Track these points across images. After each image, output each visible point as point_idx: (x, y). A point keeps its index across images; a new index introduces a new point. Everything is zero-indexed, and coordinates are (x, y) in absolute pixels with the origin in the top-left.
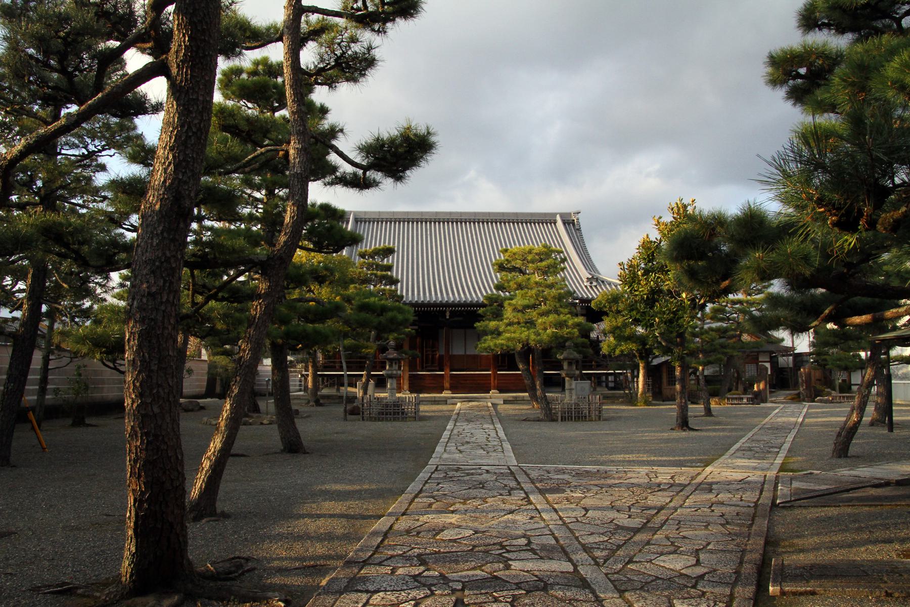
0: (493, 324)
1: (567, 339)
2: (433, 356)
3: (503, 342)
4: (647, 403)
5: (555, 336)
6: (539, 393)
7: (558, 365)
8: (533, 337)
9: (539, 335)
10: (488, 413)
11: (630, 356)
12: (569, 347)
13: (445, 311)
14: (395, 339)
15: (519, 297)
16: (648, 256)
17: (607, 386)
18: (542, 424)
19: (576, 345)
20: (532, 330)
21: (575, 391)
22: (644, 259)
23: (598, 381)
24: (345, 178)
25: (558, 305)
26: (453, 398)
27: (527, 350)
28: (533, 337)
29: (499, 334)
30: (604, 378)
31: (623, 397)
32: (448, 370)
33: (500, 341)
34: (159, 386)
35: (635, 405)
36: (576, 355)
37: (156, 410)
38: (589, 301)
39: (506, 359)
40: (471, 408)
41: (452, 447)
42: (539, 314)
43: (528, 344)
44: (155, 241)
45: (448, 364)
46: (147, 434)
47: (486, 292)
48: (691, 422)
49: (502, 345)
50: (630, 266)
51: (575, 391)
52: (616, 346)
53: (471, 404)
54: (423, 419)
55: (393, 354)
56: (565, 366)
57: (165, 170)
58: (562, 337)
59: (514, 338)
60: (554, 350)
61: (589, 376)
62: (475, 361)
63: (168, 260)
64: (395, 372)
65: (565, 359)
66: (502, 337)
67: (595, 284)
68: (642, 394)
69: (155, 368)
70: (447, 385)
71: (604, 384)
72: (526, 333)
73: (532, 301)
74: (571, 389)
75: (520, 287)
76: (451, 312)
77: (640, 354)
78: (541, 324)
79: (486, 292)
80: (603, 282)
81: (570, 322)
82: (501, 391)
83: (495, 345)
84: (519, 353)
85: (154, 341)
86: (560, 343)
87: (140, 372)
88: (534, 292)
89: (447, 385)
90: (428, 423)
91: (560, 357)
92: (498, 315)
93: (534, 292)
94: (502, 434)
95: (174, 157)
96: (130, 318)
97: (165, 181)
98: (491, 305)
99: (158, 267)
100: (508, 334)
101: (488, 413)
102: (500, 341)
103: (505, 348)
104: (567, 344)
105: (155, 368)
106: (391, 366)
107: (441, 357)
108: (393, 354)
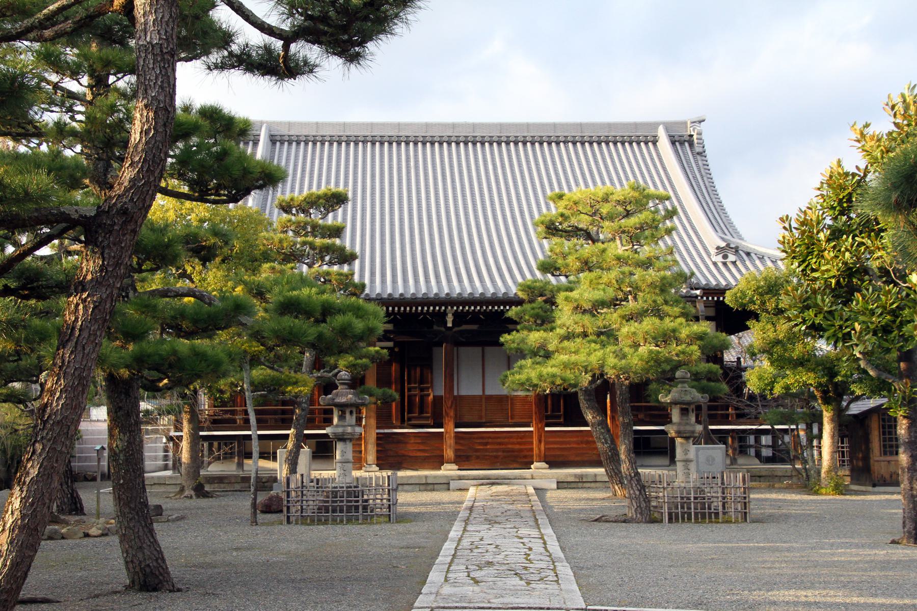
0: (535, 337)
1: (678, 366)
2: (423, 398)
3: (554, 370)
4: (840, 489)
5: (655, 360)
6: (625, 467)
7: (661, 415)
8: (612, 361)
9: (624, 356)
11: (805, 397)
12: (683, 381)
13: (445, 314)
16: (840, 202)
17: (758, 455)
20: (610, 348)
21: (696, 464)
22: (833, 208)
23: (740, 445)
25: (660, 300)
26: (460, 478)
27: (602, 387)
28: (612, 361)
29: (548, 356)
30: (752, 439)
31: (791, 477)
33: (549, 369)
35: (816, 493)
36: (695, 395)
38: (721, 292)
39: (561, 405)
40: (495, 497)
42: (623, 317)
43: (602, 375)
45: (452, 414)
49: (554, 376)
50: (803, 224)
51: (696, 464)
53: (496, 489)
54: (403, 518)
55: (344, 395)
56: (675, 415)
58: (668, 361)
59: (575, 364)
60: (653, 386)
61: (721, 437)
62: (500, 407)
64: (349, 430)
65: (674, 403)
66: (551, 362)
67: (732, 258)
68: (829, 471)
70: (449, 453)
71: (752, 451)
72: (599, 354)
73: (611, 293)
74: (687, 461)
76: (456, 314)
77: (825, 393)
80: (748, 254)
81: (684, 333)
82: (553, 464)
83: (540, 377)
84: (586, 391)
86: (667, 374)
91: (665, 398)
92: (544, 320)
93: (613, 275)
94: (554, 547)
100: (560, 356)
101: (527, 507)
102: (549, 369)
103: (558, 382)
104: (678, 374)
106: (342, 417)
108: (344, 395)
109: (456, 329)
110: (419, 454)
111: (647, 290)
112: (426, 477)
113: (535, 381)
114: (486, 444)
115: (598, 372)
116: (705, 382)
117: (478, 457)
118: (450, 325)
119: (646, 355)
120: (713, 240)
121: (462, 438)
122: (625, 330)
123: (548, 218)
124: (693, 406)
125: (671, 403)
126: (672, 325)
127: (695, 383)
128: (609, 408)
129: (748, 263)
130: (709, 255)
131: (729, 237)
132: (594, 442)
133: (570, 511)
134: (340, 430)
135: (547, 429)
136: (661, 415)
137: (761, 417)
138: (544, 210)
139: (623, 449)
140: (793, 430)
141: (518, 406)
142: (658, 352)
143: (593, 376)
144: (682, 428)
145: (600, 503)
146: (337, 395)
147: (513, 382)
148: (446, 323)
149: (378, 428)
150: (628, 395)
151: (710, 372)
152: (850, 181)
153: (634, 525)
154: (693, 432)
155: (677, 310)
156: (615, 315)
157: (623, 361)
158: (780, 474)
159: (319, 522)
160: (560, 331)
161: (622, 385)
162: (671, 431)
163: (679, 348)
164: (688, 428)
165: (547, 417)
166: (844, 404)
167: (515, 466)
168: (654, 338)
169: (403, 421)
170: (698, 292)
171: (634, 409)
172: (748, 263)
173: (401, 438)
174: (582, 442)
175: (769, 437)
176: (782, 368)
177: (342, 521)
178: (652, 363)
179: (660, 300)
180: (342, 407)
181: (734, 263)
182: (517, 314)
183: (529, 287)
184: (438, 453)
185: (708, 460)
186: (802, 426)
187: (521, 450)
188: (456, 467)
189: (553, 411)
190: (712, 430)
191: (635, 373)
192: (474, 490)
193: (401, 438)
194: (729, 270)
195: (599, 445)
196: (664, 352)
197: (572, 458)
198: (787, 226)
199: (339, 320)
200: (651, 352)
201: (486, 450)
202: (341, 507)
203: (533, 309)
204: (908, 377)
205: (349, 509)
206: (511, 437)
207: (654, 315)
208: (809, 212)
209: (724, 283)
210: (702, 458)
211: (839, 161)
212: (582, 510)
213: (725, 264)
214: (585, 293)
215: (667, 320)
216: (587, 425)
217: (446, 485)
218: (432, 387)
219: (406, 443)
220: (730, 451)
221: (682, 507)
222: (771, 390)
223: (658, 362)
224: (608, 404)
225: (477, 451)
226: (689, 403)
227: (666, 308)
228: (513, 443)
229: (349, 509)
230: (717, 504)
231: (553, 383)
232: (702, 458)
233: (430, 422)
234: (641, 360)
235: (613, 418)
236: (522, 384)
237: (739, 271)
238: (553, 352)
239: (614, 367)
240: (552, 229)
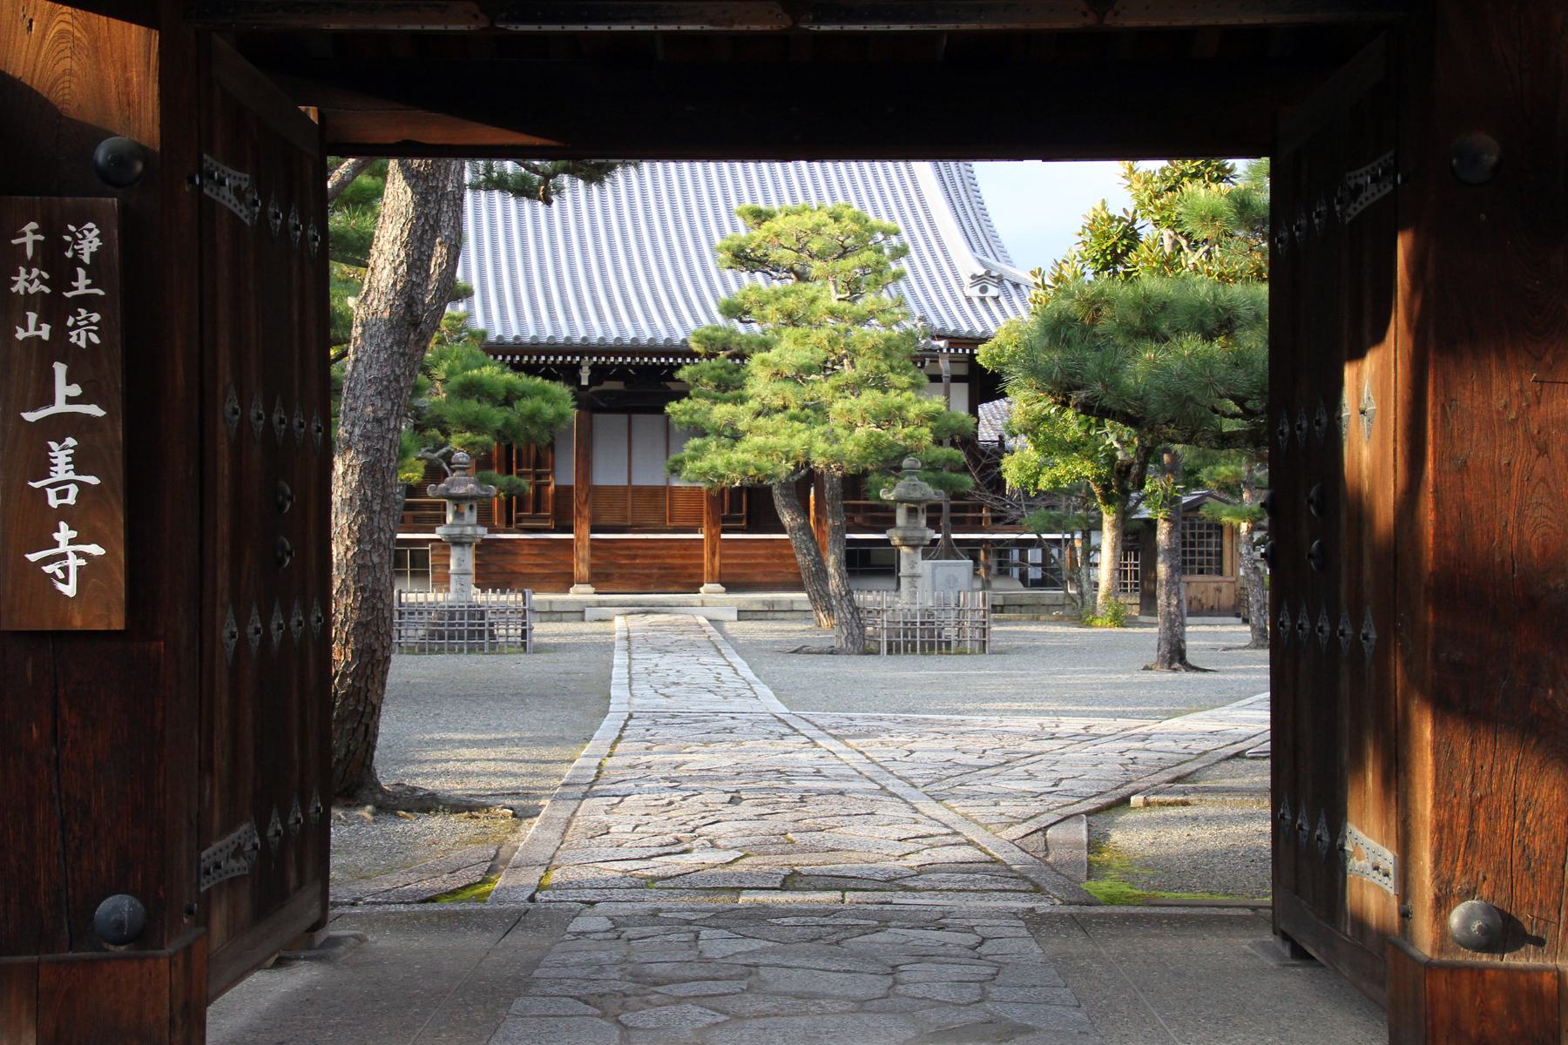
0: (721, 412)
1: (905, 453)
2: (539, 489)
3: (748, 457)
4: (1120, 619)
5: (875, 446)
6: (834, 584)
7: (882, 517)
8: (820, 446)
9: (837, 440)
10: (703, 637)
11: (1078, 489)
12: (911, 472)
13: (579, 366)
14: (469, 446)
15: (786, 344)
16: (1104, 253)
17: (1023, 578)
18: (840, 659)
19: (932, 466)
20: (819, 429)
21: (929, 583)
22: (1095, 260)
24: (506, 181)
25: (884, 367)
26: (600, 604)
27: (805, 479)
28: (820, 446)
29: (736, 437)
30: (1015, 554)
31: (1063, 606)
32: (586, 528)
33: (740, 455)
34: (381, 530)
35: (1089, 625)
36: (929, 492)
37: (376, 559)
39: (749, 504)
41: (641, 688)
42: (837, 388)
43: (807, 464)
44: (383, 355)
45: (586, 512)
46: (363, 589)
47: (697, 320)
48: (1190, 657)
49: (746, 464)
50: (1057, 280)
51: (929, 583)
52: (1041, 466)
53: (651, 618)
54: (540, 649)
55: (463, 484)
56: (901, 517)
57: (395, 270)
58: (891, 445)
59: (774, 449)
60: (874, 478)
61: (971, 549)
62: (653, 504)
63: (397, 380)
64: (469, 530)
66: (741, 446)
67: (993, 291)
68: (1107, 596)
69: (377, 508)
70: (581, 569)
71: (1016, 572)
72: (804, 436)
73: (821, 355)
75: (791, 319)
76: (594, 368)
77: (1106, 488)
78: (841, 414)
79: (697, 320)
80: (1016, 286)
81: (912, 412)
82: (731, 587)
83: (729, 464)
84: (785, 486)
85: (378, 476)
86: (892, 462)
87: (359, 513)
88: (823, 334)
89: (581, 569)
90: (562, 657)
91: (887, 495)
92: (729, 386)
93: (823, 334)
95: (407, 255)
96: (350, 448)
97: (394, 284)
98: (710, 356)
99: (387, 387)
100: (754, 436)
101: (703, 637)
102: (740, 455)
103: (752, 472)
104: (906, 463)
105: (377, 508)
106: (458, 514)
107: (564, 493)
108: (463, 484)
109: (593, 389)
110: (536, 570)
111: (869, 353)
112: (551, 602)
113: (722, 471)
114: (635, 557)
115: (802, 460)
116: (945, 473)
117: (622, 576)
118: (585, 382)
119: (864, 439)
120: (968, 265)
121: (600, 548)
122: (838, 406)
123: (737, 242)
124: (924, 506)
125: (896, 501)
126: (899, 400)
127: (931, 474)
128: (812, 507)
129: (1015, 299)
130: (961, 286)
131: (991, 260)
132: (794, 557)
133: (759, 643)
134: (457, 531)
135: (724, 536)
136: (882, 517)
137: (1026, 521)
138: (729, 231)
139: (832, 562)
140: (1067, 540)
141: (680, 505)
142: (880, 436)
143: (797, 465)
144: (909, 534)
145: (799, 635)
146: (452, 484)
147: (692, 471)
148: (579, 379)
149: (845, 498)
150: (840, 490)
151: (950, 460)
152: (1117, 229)
153: (845, 657)
154: (923, 539)
155: (905, 380)
156: (826, 386)
157: (835, 447)
158: (1047, 602)
159: (432, 651)
160: (754, 404)
161: (832, 477)
162: (893, 535)
163: (906, 430)
164: (917, 534)
165: (724, 520)
166: (1131, 504)
167: (676, 589)
168: (874, 417)
169: (509, 522)
170: (942, 343)
171: (847, 508)
172: (1015, 299)
173: (508, 546)
174: (773, 556)
175: (1039, 552)
176: (1050, 454)
177: (461, 651)
178: (871, 449)
179: (884, 367)
180: (458, 500)
181: (996, 299)
182: (691, 375)
183: (708, 338)
184: (562, 569)
185: (948, 581)
186: (1078, 536)
187: (685, 567)
188: (592, 590)
189: (731, 510)
190: (956, 540)
191: (850, 462)
192: (620, 620)
193: (508, 546)
194: (988, 310)
195: (800, 558)
196: (887, 435)
197: (759, 578)
198: (1039, 281)
199: (527, 405)
200: (870, 435)
201: (635, 566)
202: (461, 632)
203: (713, 368)
204: (1171, 471)
205: (471, 634)
206: (670, 548)
207: (876, 387)
208: (1065, 266)
209: (980, 329)
210: (940, 579)
211: (1103, 202)
212: (775, 642)
213: (983, 300)
214: (790, 351)
215: (892, 393)
216: (782, 530)
217: (580, 615)
218: (553, 471)
219: (515, 554)
220: (982, 571)
221: (905, 635)
222: (1036, 484)
223: (878, 448)
224: (812, 502)
225: (621, 566)
226: (918, 502)
227: (893, 377)
228: (673, 557)
229: (471, 634)
230: (950, 632)
231: (745, 473)
232: (940, 579)
233: (550, 524)
234: (857, 445)
235: (818, 522)
236: (705, 474)
237: (1002, 311)
238: (744, 434)
239: (823, 454)
240: (743, 259)
